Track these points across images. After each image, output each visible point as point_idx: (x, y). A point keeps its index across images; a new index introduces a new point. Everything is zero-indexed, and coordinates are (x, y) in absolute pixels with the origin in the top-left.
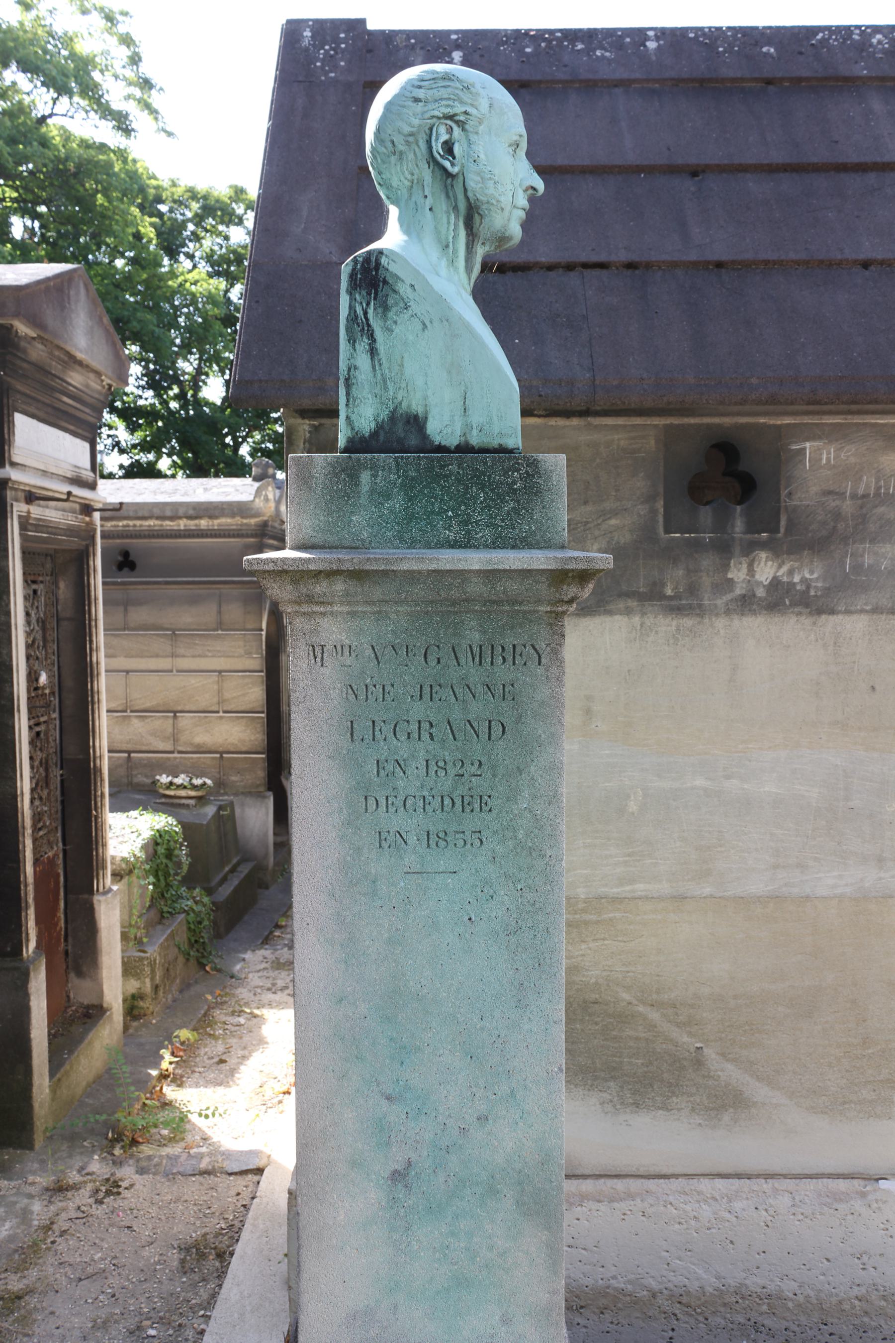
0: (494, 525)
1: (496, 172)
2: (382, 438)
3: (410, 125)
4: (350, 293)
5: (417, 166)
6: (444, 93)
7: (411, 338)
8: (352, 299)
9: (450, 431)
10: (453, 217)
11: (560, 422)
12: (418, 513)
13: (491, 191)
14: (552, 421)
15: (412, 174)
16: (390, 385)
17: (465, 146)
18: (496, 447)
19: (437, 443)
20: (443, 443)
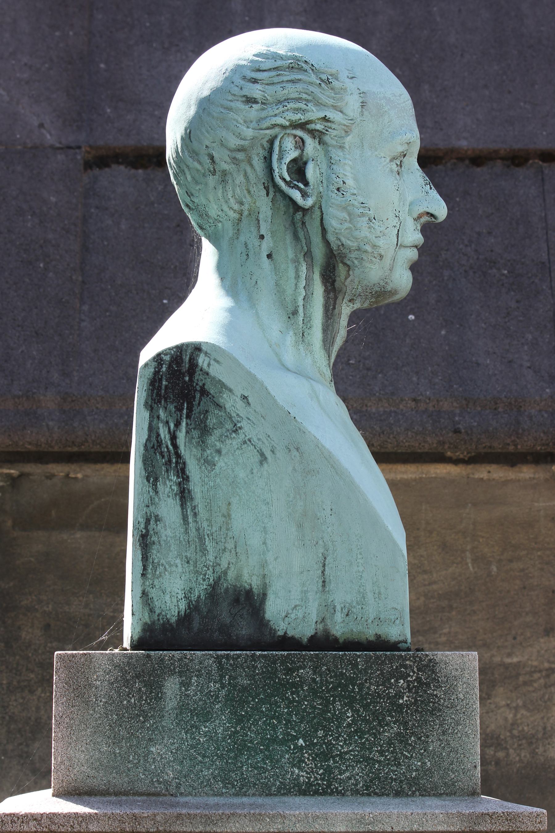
0: (367, 760)
1: (371, 203)
2: (196, 624)
3: (239, 136)
4: (151, 405)
5: (249, 192)
6: (291, 91)
7: (242, 474)
8: (154, 417)
9: (300, 615)
10: (304, 268)
11: (497, 472)
12: (251, 742)
13: (364, 233)
14: (482, 472)
15: (241, 203)
16: (209, 544)
17: (324, 166)
18: (372, 638)
19: (281, 633)
20: (290, 633)
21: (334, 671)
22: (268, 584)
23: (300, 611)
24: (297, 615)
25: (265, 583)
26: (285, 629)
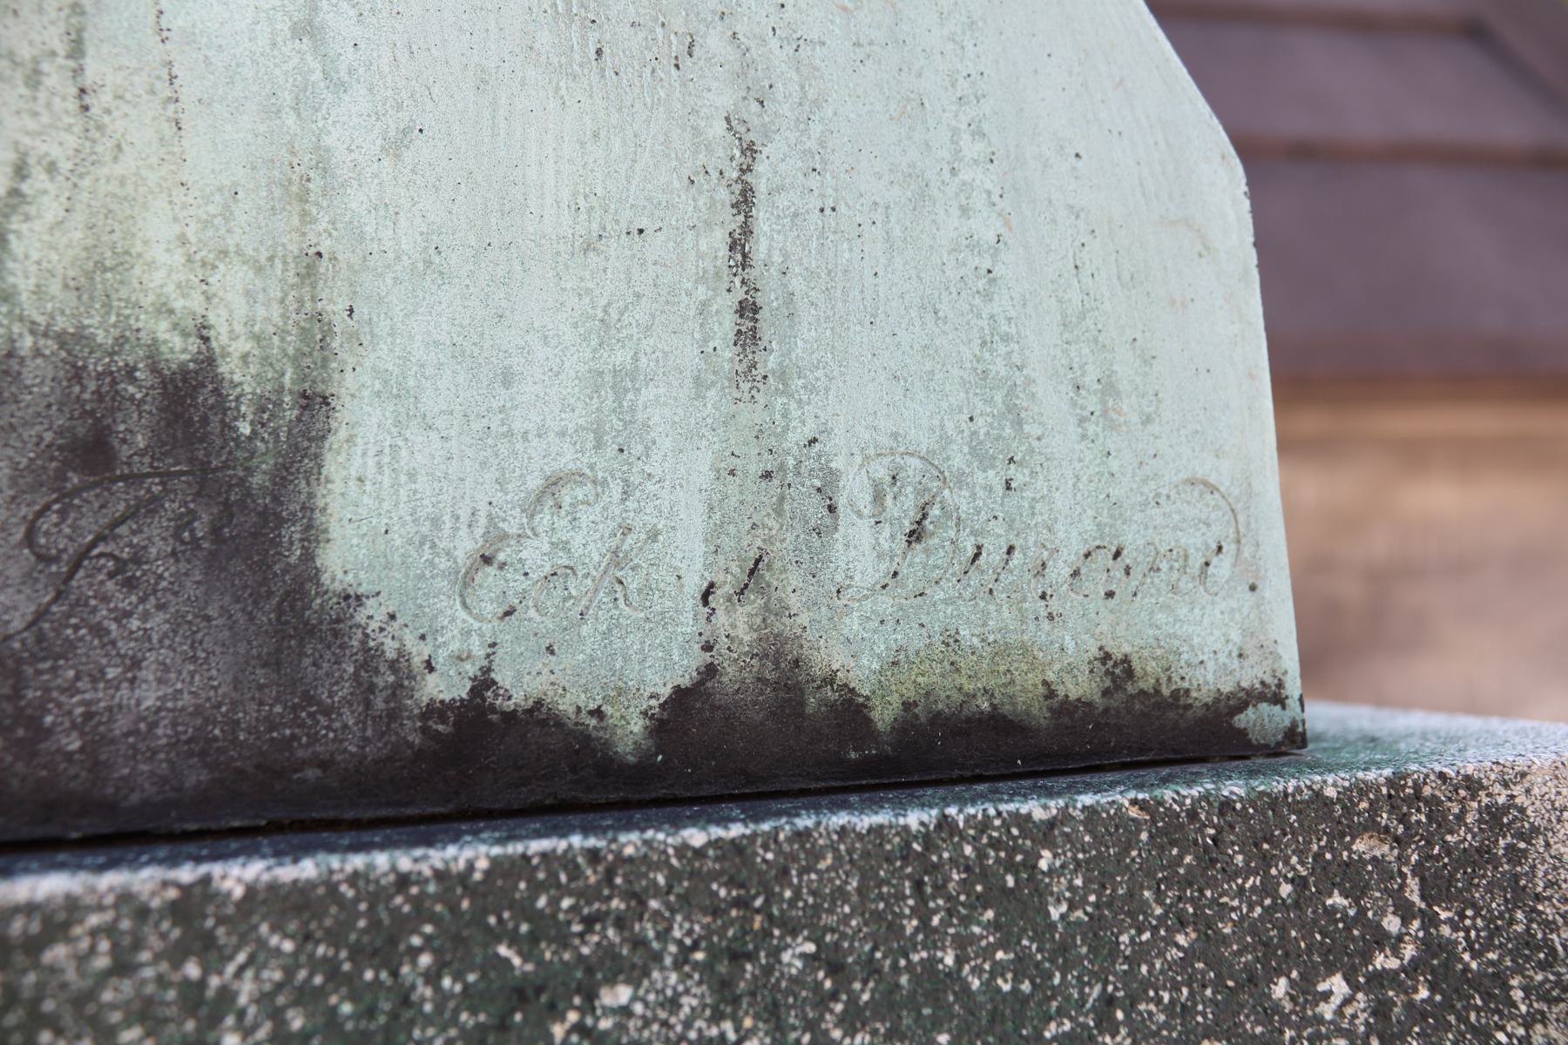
9: (589, 546)
18: (1081, 686)
19: (445, 686)
20: (519, 684)
21: (871, 968)
22: (340, 321)
23: (586, 516)
24: (565, 546)
25: (318, 317)
26: (479, 651)
